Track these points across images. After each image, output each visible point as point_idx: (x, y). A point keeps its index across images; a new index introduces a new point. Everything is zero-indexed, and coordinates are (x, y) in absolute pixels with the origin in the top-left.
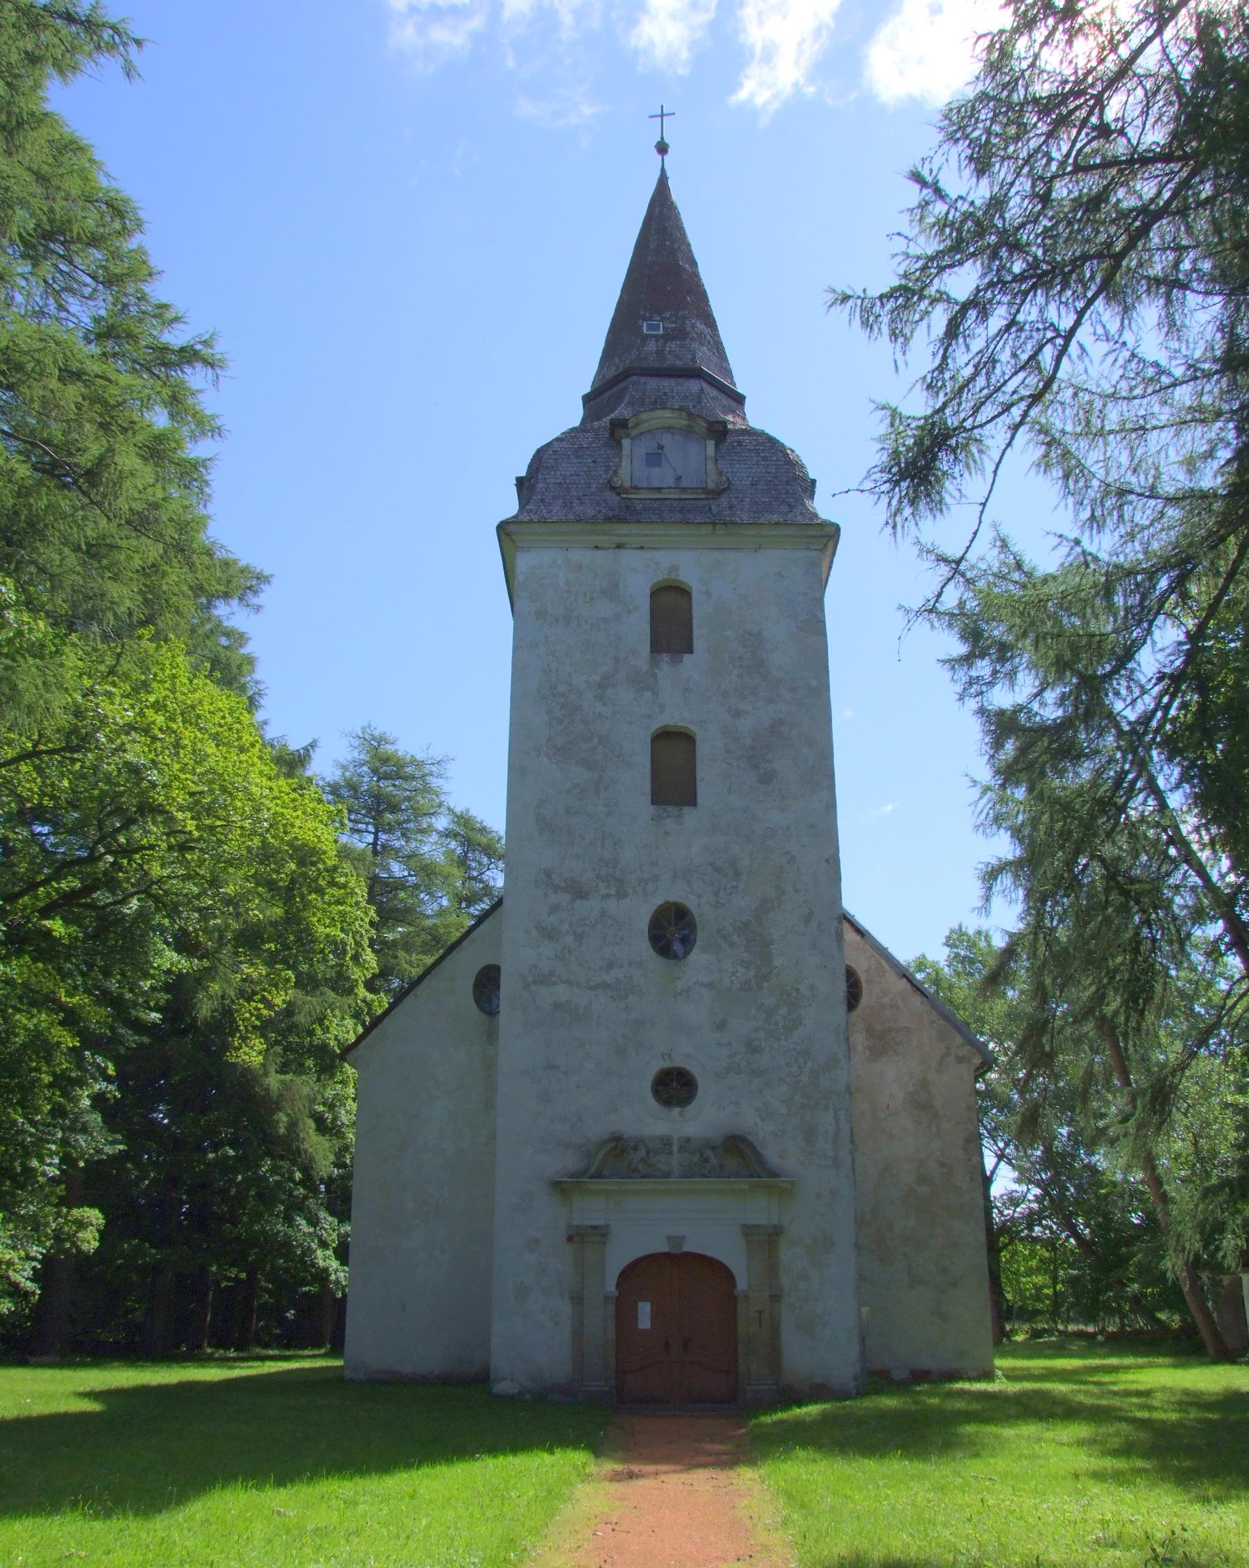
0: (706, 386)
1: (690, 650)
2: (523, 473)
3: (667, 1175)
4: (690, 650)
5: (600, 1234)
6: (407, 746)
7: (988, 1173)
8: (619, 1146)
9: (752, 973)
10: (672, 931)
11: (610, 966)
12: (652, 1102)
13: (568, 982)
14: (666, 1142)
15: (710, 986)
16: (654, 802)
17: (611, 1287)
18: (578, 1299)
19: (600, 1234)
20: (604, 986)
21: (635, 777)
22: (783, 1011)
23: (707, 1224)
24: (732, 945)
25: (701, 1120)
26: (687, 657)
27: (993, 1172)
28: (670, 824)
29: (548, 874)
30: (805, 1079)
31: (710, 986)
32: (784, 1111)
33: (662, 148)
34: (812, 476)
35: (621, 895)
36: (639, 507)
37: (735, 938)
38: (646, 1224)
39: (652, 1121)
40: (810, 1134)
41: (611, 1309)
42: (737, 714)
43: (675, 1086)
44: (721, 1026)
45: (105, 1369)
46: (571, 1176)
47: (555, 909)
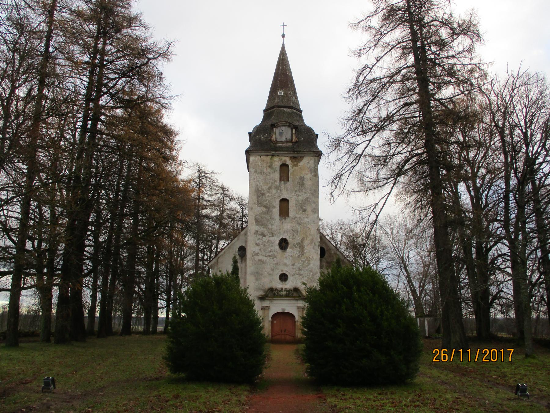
2: (251, 131)
3: (282, 296)
4: (288, 181)
6: (208, 168)
8: (271, 290)
10: (284, 244)
11: (270, 252)
12: (279, 280)
15: (291, 256)
16: (280, 216)
17: (270, 319)
19: (268, 308)
20: (269, 256)
21: (276, 211)
25: (289, 285)
28: (283, 220)
29: (257, 232)
30: (311, 276)
31: (291, 256)
34: (316, 133)
35: (273, 236)
39: (278, 285)
41: (270, 323)
42: (298, 196)
43: (284, 277)
44: (293, 265)
47: (259, 239)
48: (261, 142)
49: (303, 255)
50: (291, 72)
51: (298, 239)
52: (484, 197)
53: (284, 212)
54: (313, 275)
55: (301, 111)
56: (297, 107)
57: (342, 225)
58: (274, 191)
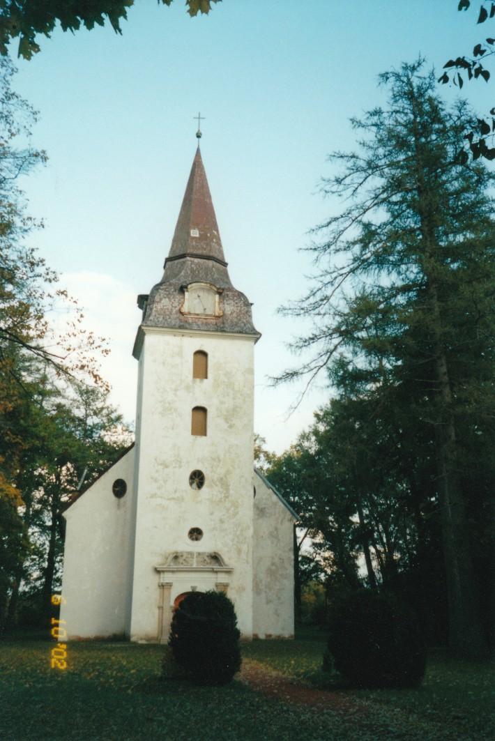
0: (215, 263)
1: (206, 377)
4: (206, 377)
5: (170, 585)
7: (298, 545)
9: (223, 495)
10: (197, 478)
11: (175, 491)
13: (161, 497)
14: (191, 554)
18: (161, 608)
19: (170, 585)
20: (174, 499)
22: (232, 509)
23: (204, 583)
24: (216, 485)
25: (205, 546)
26: (205, 380)
27: (300, 544)
30: (238, 533)
32: (231, 543)
33: (199, 136)
36: (190, 321)
37: (218, 483)
38: (183, 584)
40: (239, 551)
43: (196, 533)
45: (73, 636)
46: (160, 565)
47: (157, 471)
49: (227, 497)
50: (210, 197)
51: (221, 471)
52: (308, 302)
54: (242, 530)
55: (225, 265)
56: (215, 255)
57: (304, 437)
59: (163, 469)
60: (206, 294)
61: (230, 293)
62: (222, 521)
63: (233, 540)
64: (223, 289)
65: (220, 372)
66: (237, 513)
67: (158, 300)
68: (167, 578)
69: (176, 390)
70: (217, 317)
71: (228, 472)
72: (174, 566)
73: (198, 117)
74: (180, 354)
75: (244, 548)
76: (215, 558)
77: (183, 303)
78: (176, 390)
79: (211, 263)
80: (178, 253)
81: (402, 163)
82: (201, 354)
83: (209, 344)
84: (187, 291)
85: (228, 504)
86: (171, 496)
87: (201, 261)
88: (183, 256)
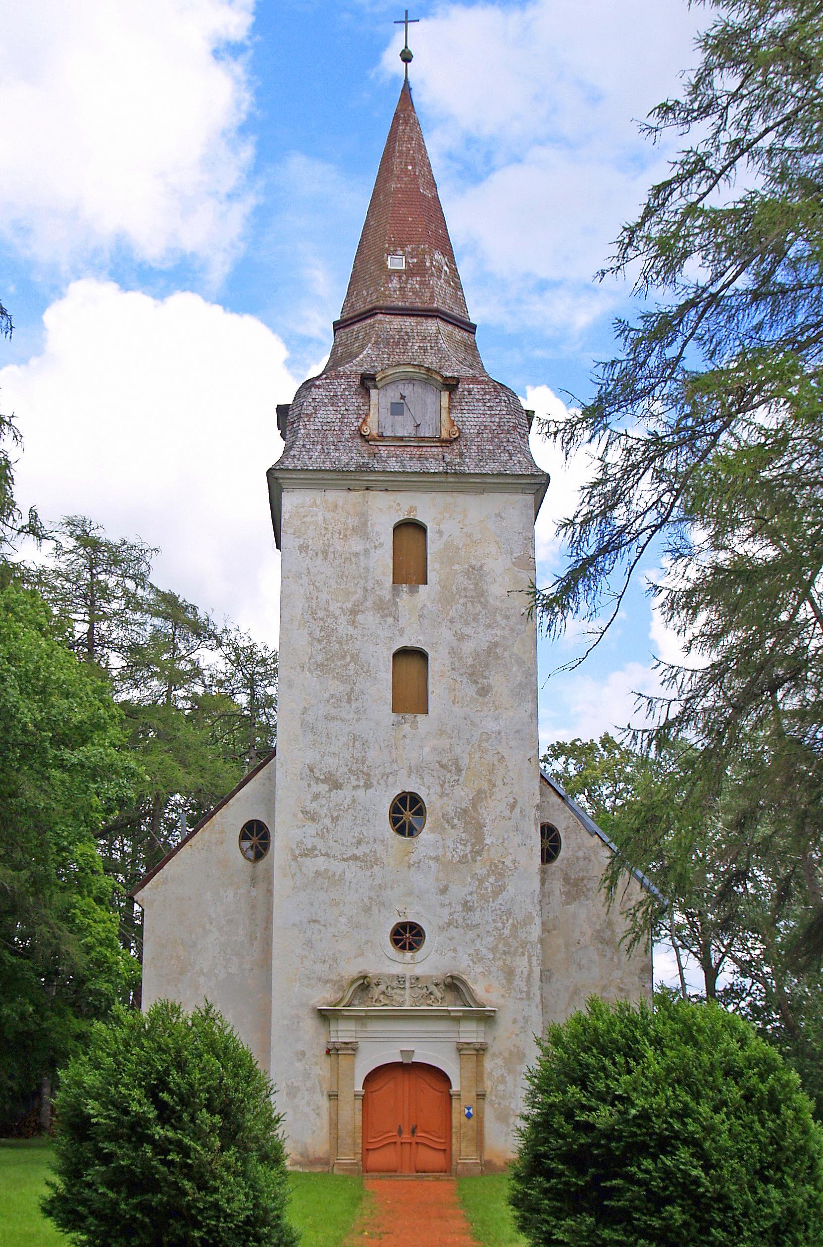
5: (351, 1048)
9: (469, 848)
10: (407, 812)
11: (359, 842)
13: (327, 855)
14: (401, 979)
19: (351, 1048)
20: (355, 858)
25: (428, 962)
30: (507, 932)
40: (510, 974)
43: (407, 936)
47: (316, 797)
48: (317, 453)
53: (410, 697)
58: (369, 619)
59: (330, 790)
60: (419, 389)
61: (475, 388)
62: (467, 907)
63: (494, 950)
64: (458, 380)
65: (456, 567)
66: (502, 889)
67: (310, 410)
68: (344, 1032)
69: (354, 612)
70: (443, 441)
71: (479, 797)
72: (359, 1008)
73: (409, 24)
74: (362, 530)
75: (521, 964)
76: (454, 985)
77: (367, 415)
78: (354, 612)
79: (432, 326)
80: (361, 307)
81: (211, 659)
82: (410, 530)
83: (425, 507)
84: (376, 387)
85: (480, 869)
86: (349, 854)
87: (410, 322)
88: (370, 313)
